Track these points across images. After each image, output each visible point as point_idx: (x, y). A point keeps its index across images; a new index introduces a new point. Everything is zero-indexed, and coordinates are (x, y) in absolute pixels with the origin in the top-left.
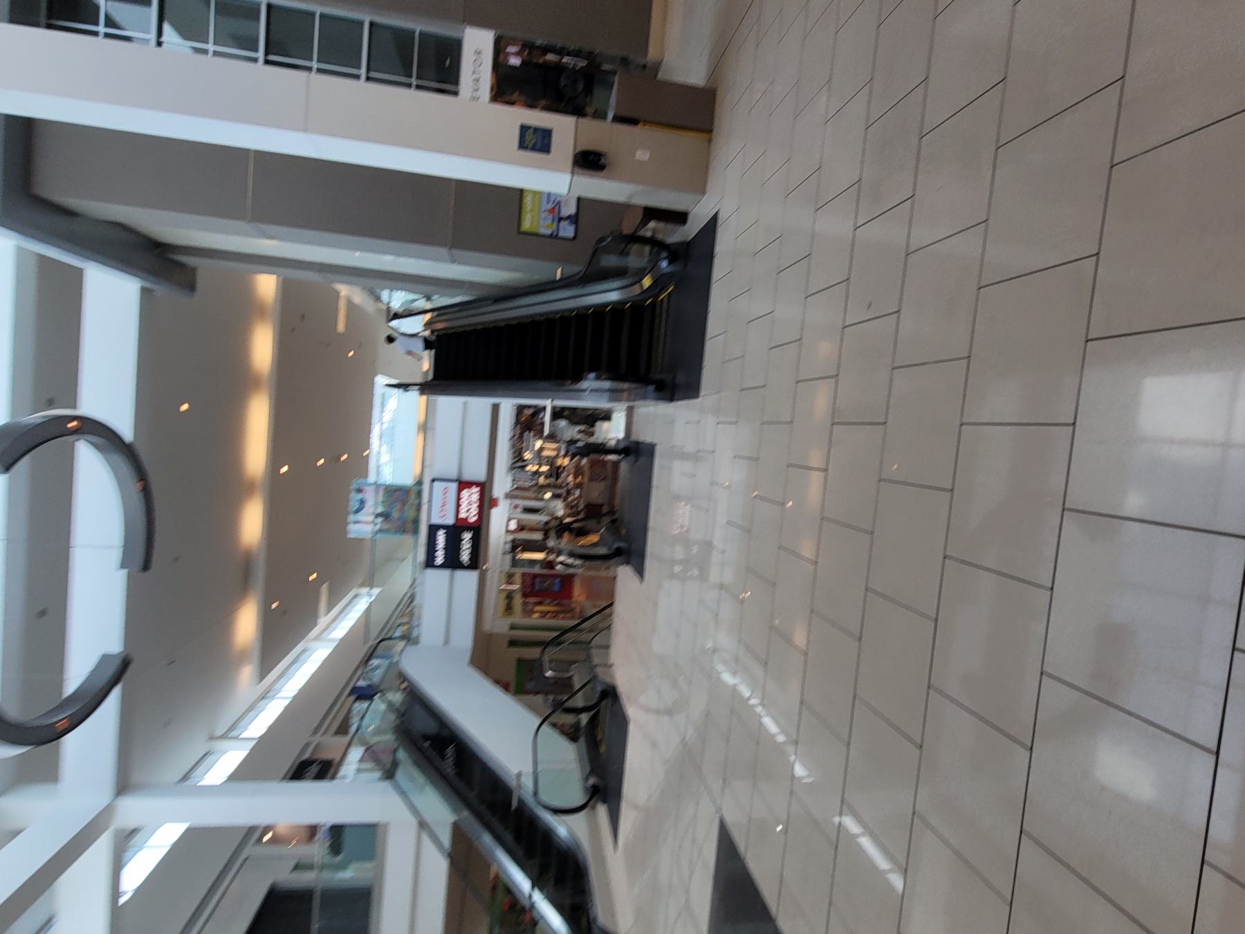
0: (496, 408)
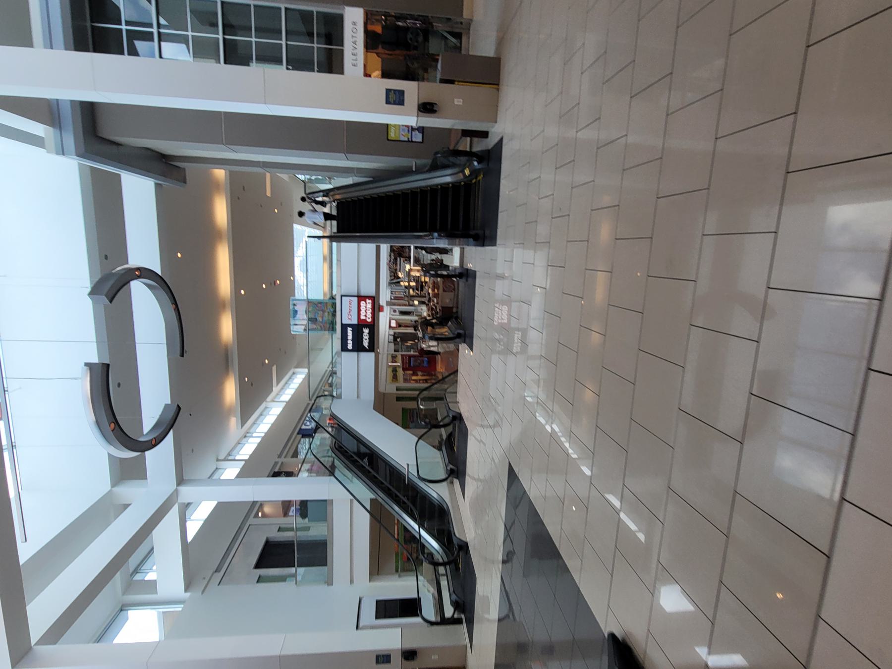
0: (378, 249)
